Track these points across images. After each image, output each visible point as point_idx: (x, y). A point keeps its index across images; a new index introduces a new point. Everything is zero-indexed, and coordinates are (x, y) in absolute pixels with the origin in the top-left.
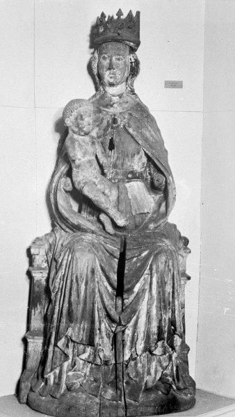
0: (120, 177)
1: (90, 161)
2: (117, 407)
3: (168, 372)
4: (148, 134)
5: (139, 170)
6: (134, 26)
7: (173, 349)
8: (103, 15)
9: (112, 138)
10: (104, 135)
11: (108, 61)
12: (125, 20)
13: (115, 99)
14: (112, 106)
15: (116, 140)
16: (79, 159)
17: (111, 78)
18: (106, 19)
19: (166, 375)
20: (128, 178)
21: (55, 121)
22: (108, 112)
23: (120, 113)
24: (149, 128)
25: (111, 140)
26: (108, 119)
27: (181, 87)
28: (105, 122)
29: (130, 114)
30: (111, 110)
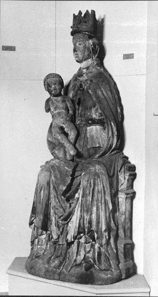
0: (84, 123)
1: (59, 113)
2: (55, 273)
3: (90, 255)
4: (100, 93)
5: (97, 118)
7: (94, 240)
8: (74, 14)
18: (83, 15)
19: (88, 257)
20: (89, 123)
23: (86, 80)
25: (79, 99)
27: (133, 58)
29: (91, 81)
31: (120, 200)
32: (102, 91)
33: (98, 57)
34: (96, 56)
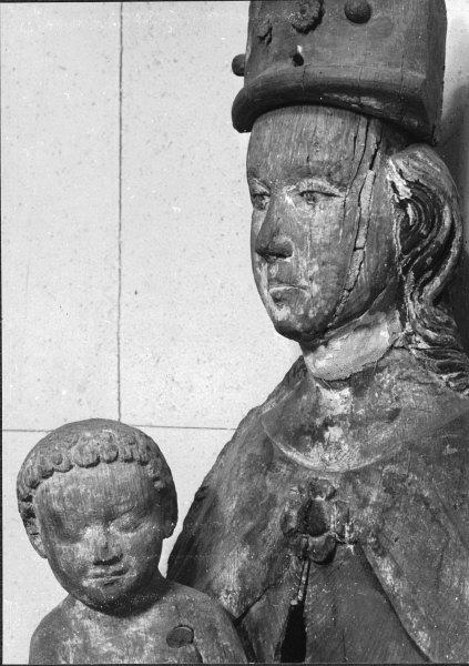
9: (301, 604)
10: (271, 585)
14: (317, 435)
23: (349, 476)
30: (312, 459)
33: (438, 299)
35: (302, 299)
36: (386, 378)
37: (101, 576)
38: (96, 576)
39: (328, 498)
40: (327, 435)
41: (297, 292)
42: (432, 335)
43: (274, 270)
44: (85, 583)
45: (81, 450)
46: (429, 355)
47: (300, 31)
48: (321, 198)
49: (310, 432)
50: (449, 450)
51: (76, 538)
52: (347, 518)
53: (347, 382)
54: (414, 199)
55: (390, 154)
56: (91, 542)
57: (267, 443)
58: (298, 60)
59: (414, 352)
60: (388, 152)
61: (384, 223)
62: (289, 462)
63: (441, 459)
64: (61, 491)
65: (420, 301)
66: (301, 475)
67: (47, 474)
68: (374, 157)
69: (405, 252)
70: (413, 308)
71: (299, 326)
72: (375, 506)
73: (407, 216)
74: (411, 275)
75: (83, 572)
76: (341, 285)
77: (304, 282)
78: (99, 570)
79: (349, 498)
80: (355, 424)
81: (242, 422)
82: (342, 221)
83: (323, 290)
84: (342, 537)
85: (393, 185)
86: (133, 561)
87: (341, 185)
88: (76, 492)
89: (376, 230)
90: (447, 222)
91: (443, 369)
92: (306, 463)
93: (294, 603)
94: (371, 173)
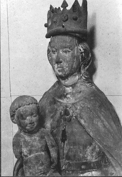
1: (36, 157)
6: (80, 15)
8: (51, 7)
9: (65, 129)
10: (58, 126)
11: (56, 54)
12: (69, 11)
13: (69, 90)
14: (65, 97)
15: (69, 130)
16: (26, 156)
17: (59, 71)
18: (69, 8)
21: (96, 73)
22: (61, 103)
23: (73, 104)
24: (102, 118)
26: (61, 110)
28: (58, 115)
30: (64, 101)
31: (93, 172)
32: (102, 121)
33: (87, 70)
34: (86, 68)
35: (64, 71)
36: (78, 85)
37: (30, 126)
38: (29, 126)
39: (70, 109)
40: (67, 96)
41: (63, 69)
42: (86, 76)
43: (59, 66)
44: (27, 128)
45: (26, 102)
46: (85, 80)
47: (63, 21)
48: (68, 52)
49: (63, 95)
50: (92, 98)
51: (25, 119)
52: (74, 112)
53: (71, 86)
54: (84, 52)
55: (79, 44)
56: (29, 120)
57: (53, 98)
58: (63, 27)
59: (82, 80)
60: (79, 44)
61: (79, 56)
62: (59, 102)
63: (91, 100)
64: (23, 110)
65: (84, 70)
66: (62, 104)
67: (20, 107)
68: (77, 44)
69: (82, 61)
70: (82, 71)
71: (64, 76)
72: (79, 109)
73: (82, 55)
74: (83, 66)
75: (27, 125)
76: (72, 68)
77: (65, 68)
78: (30, 125)
79: (74, 108)
80: (73, 94)
81: (44, 94)
82: (72, 56)
83: (69, 69)
84: (73, 115)
85: (80, 49)
86: (36, 123)
87: (72, 50)
88: (26, 110)
89: (77, 57)
90: (90, 56)
91: (88, 83)
92: (63, 102)
93: (63, 129)
94: (76, 47)
